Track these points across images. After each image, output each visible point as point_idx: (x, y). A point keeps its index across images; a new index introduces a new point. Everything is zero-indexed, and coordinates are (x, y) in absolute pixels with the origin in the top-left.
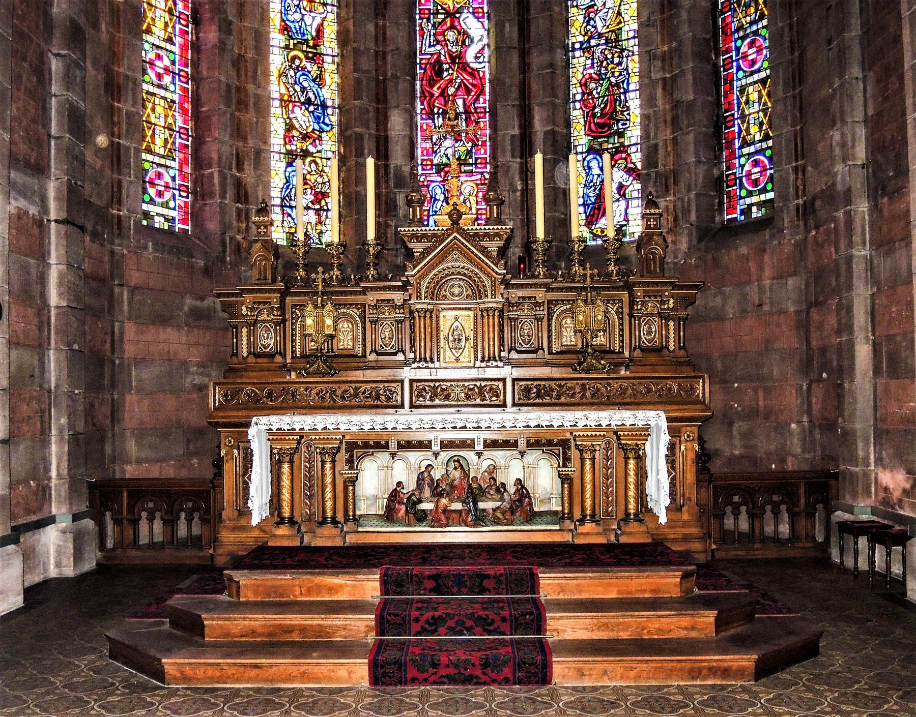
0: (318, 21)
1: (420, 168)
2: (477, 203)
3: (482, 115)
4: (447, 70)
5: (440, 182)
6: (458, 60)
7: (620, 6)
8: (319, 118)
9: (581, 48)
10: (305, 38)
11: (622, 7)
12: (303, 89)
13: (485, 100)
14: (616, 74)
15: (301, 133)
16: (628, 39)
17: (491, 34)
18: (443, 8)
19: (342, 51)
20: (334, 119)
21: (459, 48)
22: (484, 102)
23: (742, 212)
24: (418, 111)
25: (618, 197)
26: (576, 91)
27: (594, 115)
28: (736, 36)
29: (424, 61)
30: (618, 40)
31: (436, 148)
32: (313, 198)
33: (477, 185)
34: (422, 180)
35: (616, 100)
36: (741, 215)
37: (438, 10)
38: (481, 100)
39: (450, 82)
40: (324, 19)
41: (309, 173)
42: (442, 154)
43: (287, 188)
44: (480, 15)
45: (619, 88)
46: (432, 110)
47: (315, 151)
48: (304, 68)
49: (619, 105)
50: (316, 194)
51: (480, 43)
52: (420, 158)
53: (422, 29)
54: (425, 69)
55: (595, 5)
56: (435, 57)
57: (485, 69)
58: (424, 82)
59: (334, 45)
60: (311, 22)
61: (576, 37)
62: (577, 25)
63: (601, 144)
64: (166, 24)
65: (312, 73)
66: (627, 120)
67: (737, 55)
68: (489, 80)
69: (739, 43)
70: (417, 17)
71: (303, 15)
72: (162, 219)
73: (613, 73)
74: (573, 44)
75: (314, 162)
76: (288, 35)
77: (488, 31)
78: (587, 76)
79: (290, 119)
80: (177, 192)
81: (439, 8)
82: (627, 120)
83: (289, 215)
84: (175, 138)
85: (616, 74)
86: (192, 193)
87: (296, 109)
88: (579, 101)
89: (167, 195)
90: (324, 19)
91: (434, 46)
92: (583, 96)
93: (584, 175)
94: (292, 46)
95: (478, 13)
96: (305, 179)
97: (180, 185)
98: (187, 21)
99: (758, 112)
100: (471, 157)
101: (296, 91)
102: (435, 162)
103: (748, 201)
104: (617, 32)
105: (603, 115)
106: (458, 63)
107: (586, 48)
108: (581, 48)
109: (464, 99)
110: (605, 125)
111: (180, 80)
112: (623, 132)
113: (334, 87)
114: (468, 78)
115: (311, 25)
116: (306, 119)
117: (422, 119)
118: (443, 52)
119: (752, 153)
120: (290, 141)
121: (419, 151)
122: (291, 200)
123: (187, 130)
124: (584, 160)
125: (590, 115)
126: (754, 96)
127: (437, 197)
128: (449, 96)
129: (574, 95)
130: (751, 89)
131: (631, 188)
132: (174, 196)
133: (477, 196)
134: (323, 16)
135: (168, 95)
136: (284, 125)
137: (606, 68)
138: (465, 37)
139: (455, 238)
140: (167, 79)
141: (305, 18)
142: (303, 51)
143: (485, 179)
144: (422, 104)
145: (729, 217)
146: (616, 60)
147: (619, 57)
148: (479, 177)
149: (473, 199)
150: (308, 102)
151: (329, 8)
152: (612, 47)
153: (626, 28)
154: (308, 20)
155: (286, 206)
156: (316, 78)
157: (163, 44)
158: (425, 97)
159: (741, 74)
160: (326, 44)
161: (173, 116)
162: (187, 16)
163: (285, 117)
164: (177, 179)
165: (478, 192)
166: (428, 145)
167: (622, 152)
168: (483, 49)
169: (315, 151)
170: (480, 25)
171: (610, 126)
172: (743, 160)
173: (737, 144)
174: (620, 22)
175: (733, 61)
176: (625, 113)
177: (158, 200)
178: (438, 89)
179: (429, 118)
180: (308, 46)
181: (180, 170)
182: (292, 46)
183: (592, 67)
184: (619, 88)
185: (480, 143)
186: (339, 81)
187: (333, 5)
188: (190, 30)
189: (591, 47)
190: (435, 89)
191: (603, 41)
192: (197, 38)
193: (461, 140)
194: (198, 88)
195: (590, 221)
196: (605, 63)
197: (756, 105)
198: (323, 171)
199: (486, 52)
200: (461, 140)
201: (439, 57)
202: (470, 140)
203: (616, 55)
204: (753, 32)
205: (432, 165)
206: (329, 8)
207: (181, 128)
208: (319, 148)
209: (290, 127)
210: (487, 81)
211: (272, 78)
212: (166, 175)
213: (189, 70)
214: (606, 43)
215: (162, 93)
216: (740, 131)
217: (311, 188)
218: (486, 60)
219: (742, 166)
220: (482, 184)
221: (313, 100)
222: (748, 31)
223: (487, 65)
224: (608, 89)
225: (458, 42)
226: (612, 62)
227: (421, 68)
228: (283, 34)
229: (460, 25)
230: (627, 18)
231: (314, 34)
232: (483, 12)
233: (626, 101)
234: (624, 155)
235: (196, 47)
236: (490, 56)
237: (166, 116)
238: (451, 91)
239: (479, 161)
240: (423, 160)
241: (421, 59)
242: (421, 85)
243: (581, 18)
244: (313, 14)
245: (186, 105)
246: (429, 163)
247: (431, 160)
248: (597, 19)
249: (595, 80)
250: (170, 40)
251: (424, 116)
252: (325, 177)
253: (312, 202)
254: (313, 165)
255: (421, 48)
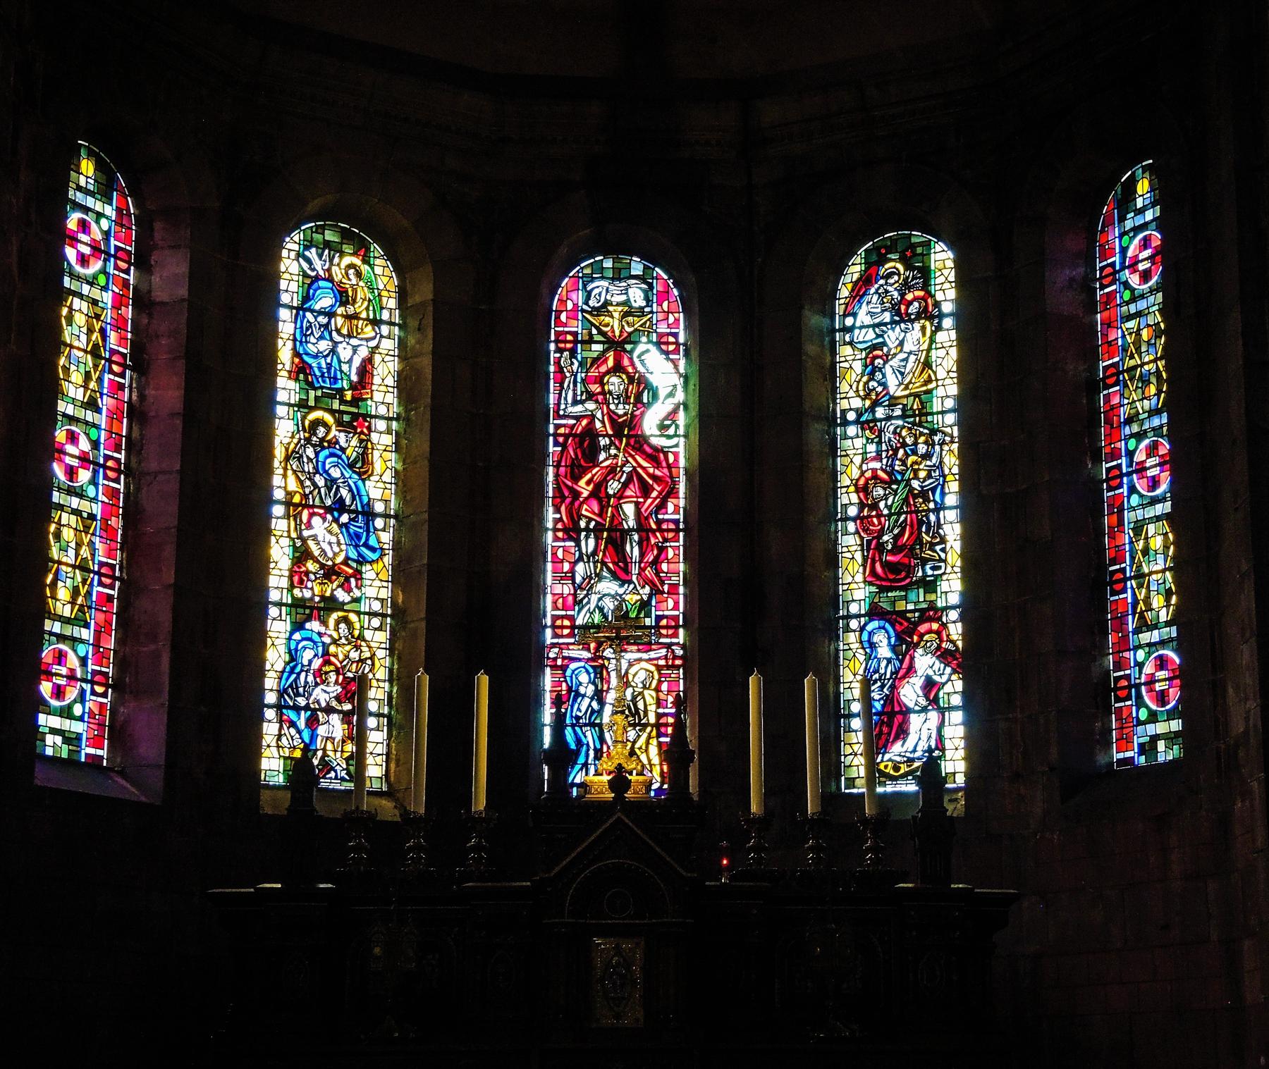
0: (363, 352)
1: (549, 632)
2: (659, 703)
3: (671, 535)
4: (607, 448)
5: (588, 660)
6: (627, 430)
7: (929, 350)
8: (358, 536)
9: (857, 422)
10: (339, 386)
11: (933, 353)
12: (331, 482)
13: (677, 507)
14: (922, 474)
15: (322, 566)
16: (943, 413)
17: (691, 387)
18: (600, 332)
19: (407, 411)
20: (386, 537)
21: (629, 408)
22: (675, 510)
23: (1142, 749)
24: (550, 525)
25: (923, 702)
26: (849, 500)
27: (880, 547)
28: (1127, 430)
29: (562, 431)
30: (924, 412)
31: (581, 594)
32: (340, 689)
33: (659, 668)
34: (552, 655)
35: (921, 523)
36: (1140, 754)
37: (590, 335)
38: (671, 507)
39: (612, 470)
40: (373, 351)
41: (335, 642)
42: (592, 606)
43: (291, 672)
44: (672, 348)
45: (927, 500)
46: (577, 524)
47: (347, 599)
48: (334, 443)
49: (927, 533)
50: (346, 683)
51: (671, 400)
52: (550, 612)
53: (560, 370)
54: (564, 445)
55: (884, 344)
56: (584, 422)
57: (680, 450)
58: (562, 470)
59: (390, 398)
60: (350, 355)
61: (850, 401)
62: (852, 377)
63: (893, 602)
64: (88, 376)
65: (349, 452)
66: (941, 560)
67: (1130, 465)
68: (686, 469)
69: (1132, 443)
70: (552, 347)
71: (336, 344)
72: (59, 740)
73: (916, 472)
74: (844, 412)
75: (346, 620)
76: (306, 381)
77: (686, 378)
78: (869, 474)
79: (304, 540)
80: (87, 687)
81: (594, 331)
82: (941, 560)
83: (292, 724)
84: (91, 585)
85: (922, 474)
86: (113, 687)
87: (316, 521)
88: (854, 519)
89: (71, 694)
90: (373, 351)
91: (582, 402)
92: (861, 510)
93: (862, 658)
94: (312, 403)
95: (668, 343)
96: (326, 653)
97: (94, 673)
98: (123, 366)
99: (1163, 571)
100: (648, 615)
101: (315, 486)
102: (579, 622)
103: (1151, 729)
104: (923, 397)
105: (897, 549)
106: (628, 437)
107: (867, 423)
108: (857, 422)
109: (637, 504)
110: (899, 566)
111: (106, 477)
112: (934, 582)
113: (388, 477)
114: (645, 464)
115: (350, 361)
116: (334, 539)
117: (556, 539)
118: (599, 415)
119: (1155, 644)
120: (301, 582)
121: (549, 598)
122: (298, 695)
123: (112, 567)
124: (862, 629)
125: (873, 548)
126: (1157, 543)
127: (582, 690)
128: (609, 497)
129: (845, 506)
130: (1151, 529)
131: (948, 688)
132: (83, 692)
133: (658, 690)
134: (373, 344)
135: (85, 506)
136: (289, 551)
137: (904, 463)
138: (640, 389)
139: (619, 820)
140: (84, 476)
141: (340, 349)
142: (332, 412)
143: (675, 657)
144: (557, 510)
145: (1121, 756)
146: (922, 449)
147: (926, 443)
148: (663, 652)
149: (650, 695)
150: (340, 506)
151: (385, 330)
152: (914, 424)
153: (940, 392)
154: (344, 352)
155: (289, 707)
156: (356, 461)
157: (80, 413)
158: (563, 498)
159: (1135, 500)
160: (378, 397)
161: (91, 543)
162: (124, 356)
163: (294, 535)
164: (90, 662)
165: (660, 682)
166: (567, 589)
167: (931, 620)
168: (675, 411)
169: (347, 599)
170: (670, 365)
171: (910, 570)
172: (1141, 655)
173: (1131, 624)
174: (929, 381)
175: (1121, 476)
176: (938, 548)
177: (55, 703)
178: (588, 483)
179: (570, 539)
180: (343, 402)
181: (96, 645)
182: (312, 403)
183: (878, 458)
184: (927, 500)
185: (666, 588)
186: (399, 467)
187: (391, 324)
188: (127, 382)
189: (875, 420)
190: (582, 483)
191: (898, 412)
192: (142, 397)
193: (630, 582)
194: (138, 489)
195: (876, 744)
196: (901, 452)
197: (1160, 558)
198: (361, 637)
199: (681, 418)
200: (630, 582)
201: (591, 422)
202: (647, 582)
203: (922, 439)
204: (1154, 429)
205: (573, 627)
206: (385, 330)
207: (101, 564)
208: (357, 593)
209: (301, 555)
210: (682, 472)
211: (276, 464)
212: (71, 654)
213: (122, 456)
214: (904, 416)
215: (75, 502)
216: (1136, 602)
217: (337, 671)
218: (681, 431)
219: (1140, 665)
220: (668, 667)
221: (348, 502)
222: (1146, 426)
223: (682, 440)
224: (906, 500)
225: (628, 397)
226: (914, 452)
227: (556, 444)
228: (297, 379)
229: (632, 364)
230: (941, 373)
231: (354, 378)
232: (677, 343)
233: (939, 526)
234: (935, 626)
235: (136, 413)
236: (687, 426)
237: (79, 545)
238: (613, 487)
239: (664, 622)
240: (555, 618)
241: (557, 427)
242: (557, 475)
243: (858, 366)
244: (354, 342)
245: (113, 522)
246: (567, 623)
247: (572, 619)
248: (888, 370)
249: (883, 481)
250: (92, 405)
251: (560, 534)
252: (365, 649)
253: (338, 698)
254: (342, 626)
255: (558, 404)
